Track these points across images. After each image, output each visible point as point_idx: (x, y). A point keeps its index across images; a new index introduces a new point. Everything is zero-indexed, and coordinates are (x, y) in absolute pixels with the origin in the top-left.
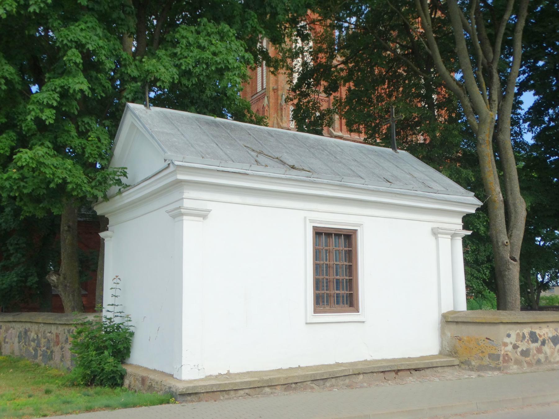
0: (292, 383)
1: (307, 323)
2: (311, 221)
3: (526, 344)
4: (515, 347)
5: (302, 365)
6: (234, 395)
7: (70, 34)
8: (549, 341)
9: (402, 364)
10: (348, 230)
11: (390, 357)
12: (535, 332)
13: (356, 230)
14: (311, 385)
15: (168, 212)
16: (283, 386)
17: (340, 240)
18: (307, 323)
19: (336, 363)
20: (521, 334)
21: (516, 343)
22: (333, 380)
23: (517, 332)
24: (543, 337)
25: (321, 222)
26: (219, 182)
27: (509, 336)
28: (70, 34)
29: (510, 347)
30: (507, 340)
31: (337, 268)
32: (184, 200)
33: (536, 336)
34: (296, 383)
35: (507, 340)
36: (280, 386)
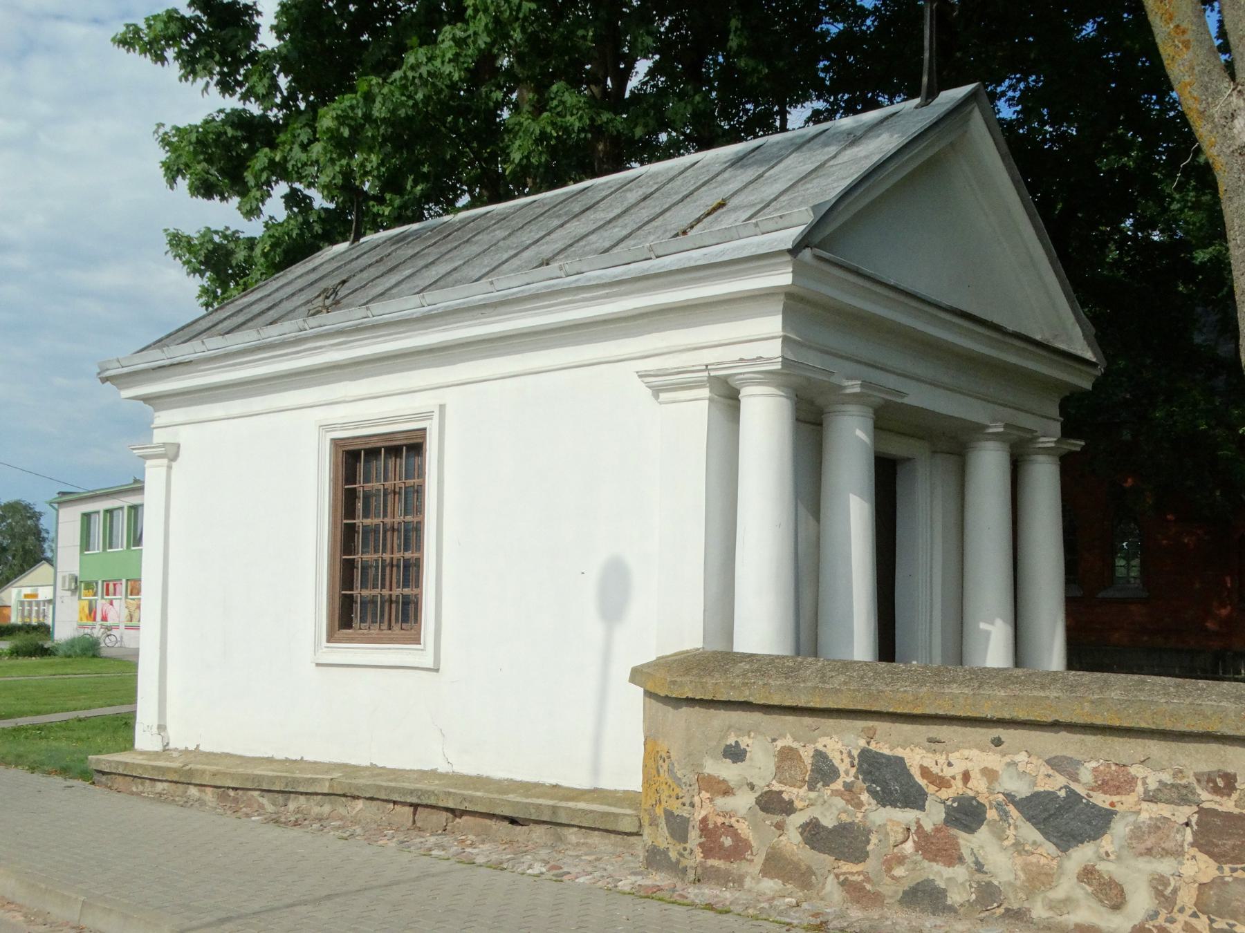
0: (228, 788)
1: (318, 665)
2: (326, 428)
3: (840, 802)
4: (772, 804)
5: (309, 757)
6: (150, 789)
7: (181, 152)
8: (1005, 815)
9: (450, 793)
10: (409, 434)
11: (498, 772)
12: (902, 759)
13: (424, 430)
14: (261, 799)
15: (642, 375)
16: (215, 789)
17: (378, 463)
18: (318, 665)
19: (371, 764)
20: (807, 755)
21: (776, 787)
22: (302, 799)
23: (780, 744)
24: (957, 788)
25: (344, 426)
26: (234, 378)
27: (736, 754)
28: (181, 152)
29: (743, 801)
30: (727, 771)
31: (406, 531)
32: (155, 431)
33: (910, 776)
34: (395, 803)
35: (727, 771)
36: (211, 789)
